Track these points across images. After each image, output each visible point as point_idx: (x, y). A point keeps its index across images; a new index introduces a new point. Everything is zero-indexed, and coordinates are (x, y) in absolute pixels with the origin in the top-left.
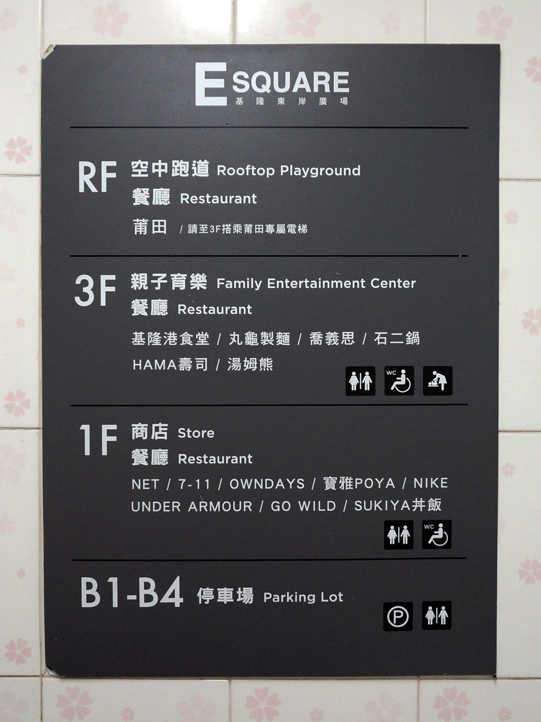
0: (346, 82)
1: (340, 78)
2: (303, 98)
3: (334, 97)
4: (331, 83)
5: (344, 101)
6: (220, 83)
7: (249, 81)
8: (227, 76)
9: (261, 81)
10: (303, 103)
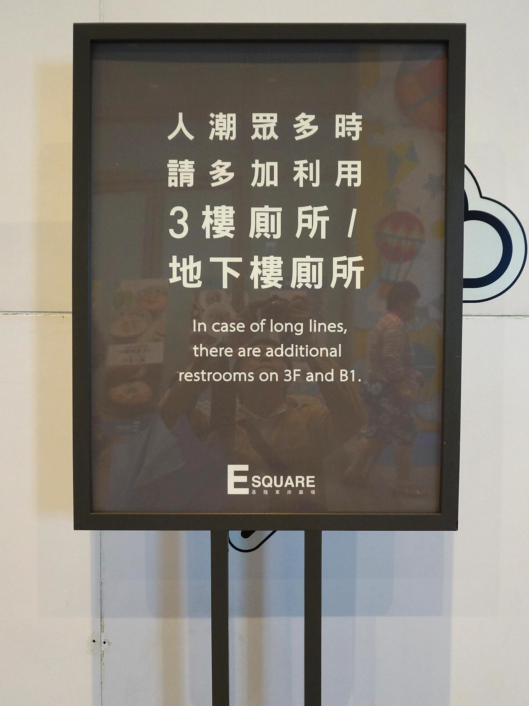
0: (313, 481)
1: (310, 479)
2: (290, 490)
3: (307, 490)
4: (305, 482)
5: (313, 492)
6: (244, 479)
7: (261, 481)
8: (249, 474)
9: (267, 481)
10: (290, 494)
